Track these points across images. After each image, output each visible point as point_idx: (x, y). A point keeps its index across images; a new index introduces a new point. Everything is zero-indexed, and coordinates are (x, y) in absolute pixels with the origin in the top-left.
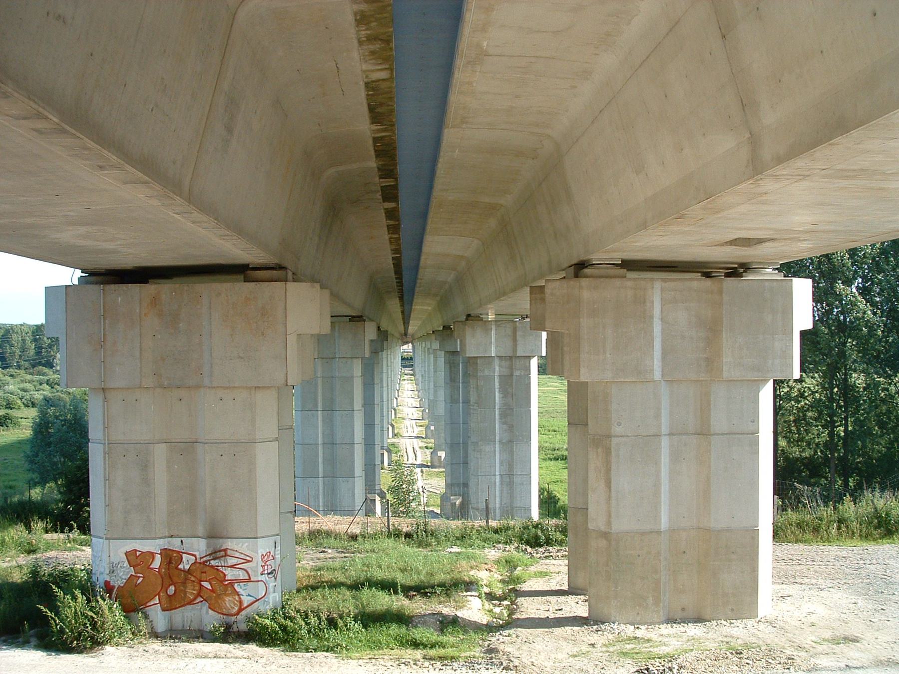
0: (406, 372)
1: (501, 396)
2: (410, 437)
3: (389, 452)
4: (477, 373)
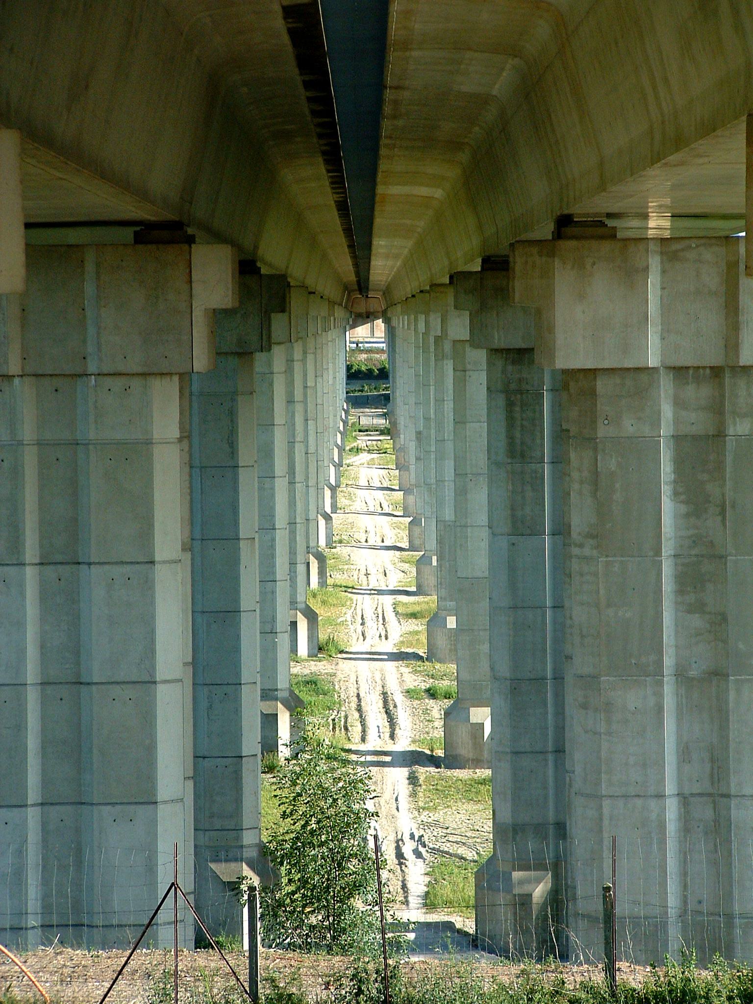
0: (364, 421)
1: (683, 509)
2: (373, 656)
3: (295, 705)
4: (595, 430)
